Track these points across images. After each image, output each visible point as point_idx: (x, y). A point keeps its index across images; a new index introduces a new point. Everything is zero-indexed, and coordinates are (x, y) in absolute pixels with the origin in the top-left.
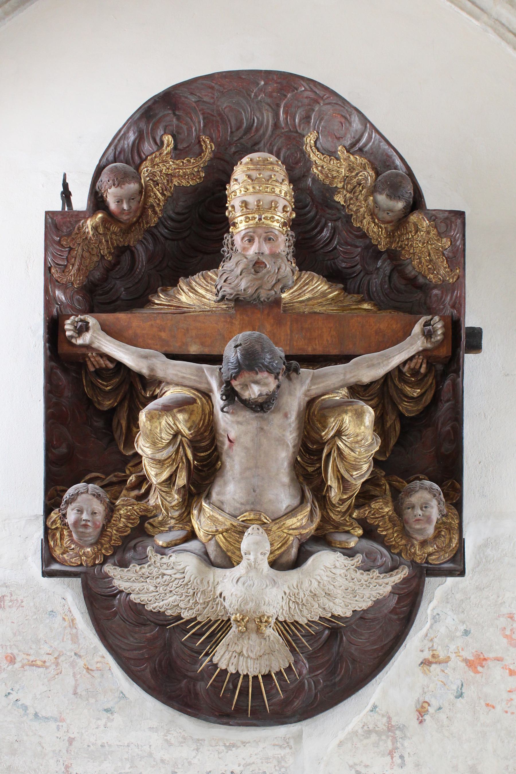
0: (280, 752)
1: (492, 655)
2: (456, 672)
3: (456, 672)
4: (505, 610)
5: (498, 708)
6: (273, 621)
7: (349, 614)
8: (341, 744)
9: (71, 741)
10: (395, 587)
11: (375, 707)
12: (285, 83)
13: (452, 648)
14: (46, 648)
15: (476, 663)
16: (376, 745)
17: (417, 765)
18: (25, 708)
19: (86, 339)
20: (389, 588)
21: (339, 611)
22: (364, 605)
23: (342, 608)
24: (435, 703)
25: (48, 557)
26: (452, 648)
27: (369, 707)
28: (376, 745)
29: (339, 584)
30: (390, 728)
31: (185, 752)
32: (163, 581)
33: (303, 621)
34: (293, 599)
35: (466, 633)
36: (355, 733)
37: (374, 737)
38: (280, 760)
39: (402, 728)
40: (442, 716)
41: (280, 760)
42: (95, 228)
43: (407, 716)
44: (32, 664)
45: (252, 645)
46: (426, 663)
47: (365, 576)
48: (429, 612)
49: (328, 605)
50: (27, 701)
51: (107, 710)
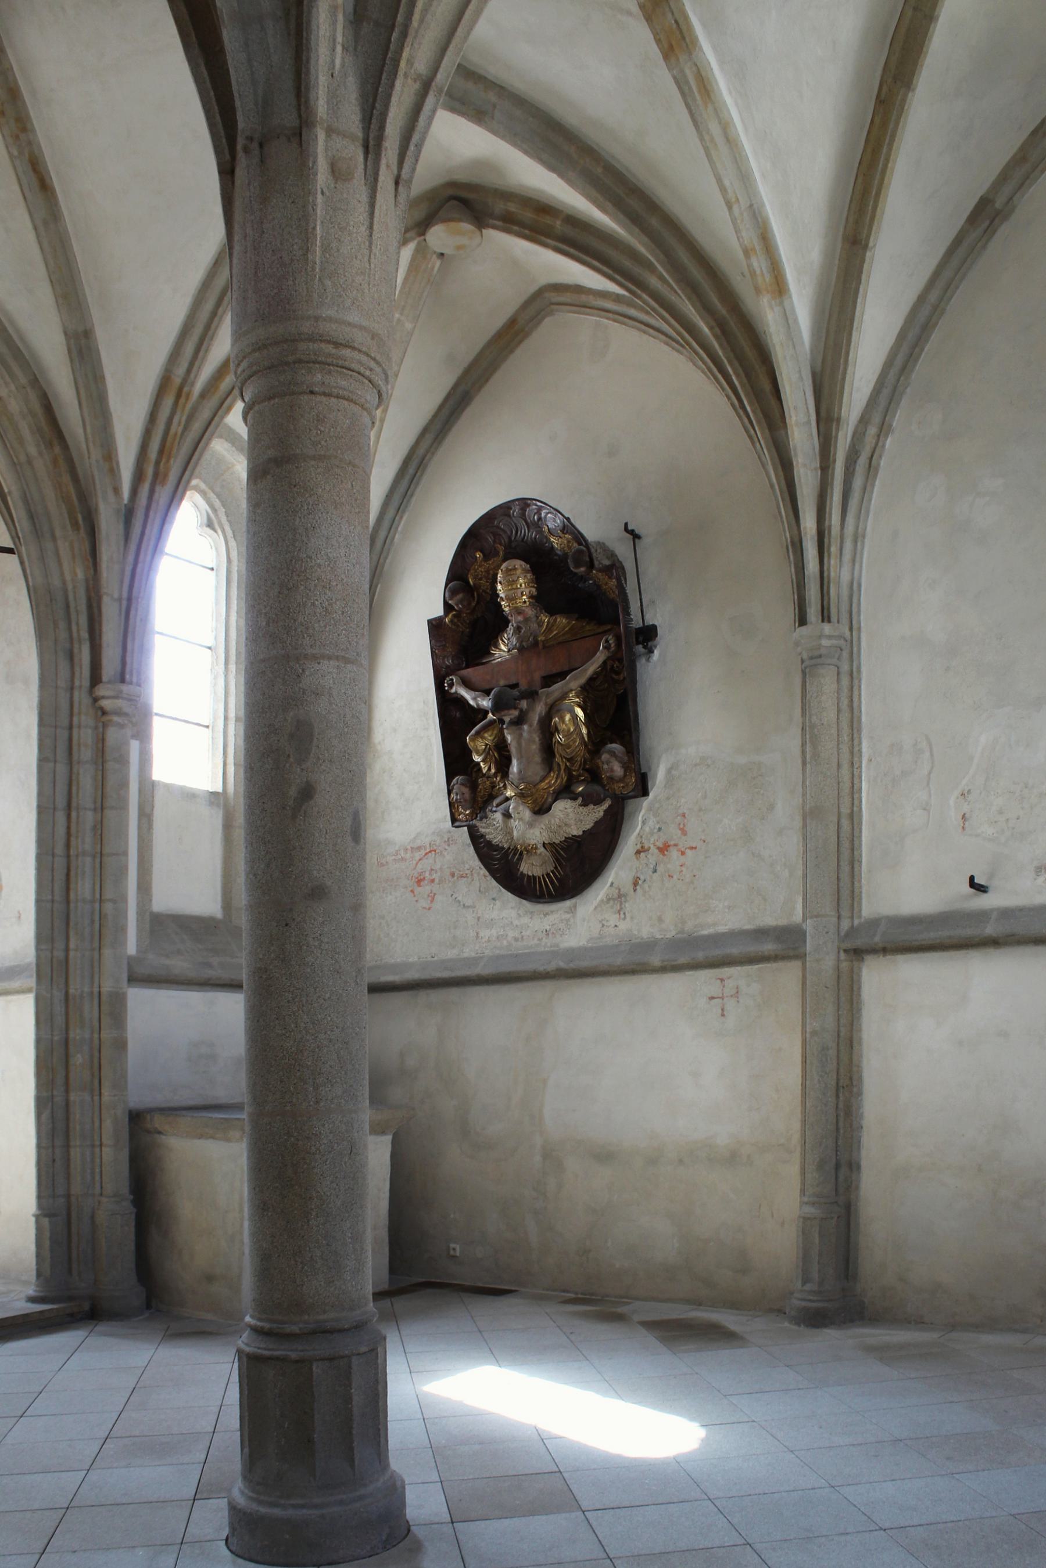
0: (568, 916)
1: (672, 843)
2: (653, 856)
3: (653, 856)
4: (680, 812)
5: (675, 877)
6: (540, 846)
7: (581, 833)
8: (596, 908)
9: (479, 918)
10: (605, 811)
11: (612, 884)
12: (504, 509)
13: (652, 840)
14: (467, 866)
15: (664, 849)
16: (612, 907)
17: (632, 918)
18: (459, 902)
19: (453, 690)
20: (602, 814)
21: (575, 833)
22: (588, 826)
23: (576, 831)
24: (642, 878)
25: (454, 820)
26: (652, 840)
27: (609, 884)
28: (612, 907)
29: (571, 818)
30: (620, 896)
31: (525, 920)
32: (493, 826)
33: (557, 842)
34: (549, 828)
35: (660, 829)
36: (602, 901)
37: (611, 902)
38: (568, 920)
39: (625, 896)
40: (646, 886)
41: (568, 920)
42: (451, 621)
43: (628, 888)
44: (462, 877)
45: (535, 860)
46: (638, 852)
47: (585, 809)
48: (640, 818)
49: (568, 830)
50: (460, 898)
51: (494, 899)
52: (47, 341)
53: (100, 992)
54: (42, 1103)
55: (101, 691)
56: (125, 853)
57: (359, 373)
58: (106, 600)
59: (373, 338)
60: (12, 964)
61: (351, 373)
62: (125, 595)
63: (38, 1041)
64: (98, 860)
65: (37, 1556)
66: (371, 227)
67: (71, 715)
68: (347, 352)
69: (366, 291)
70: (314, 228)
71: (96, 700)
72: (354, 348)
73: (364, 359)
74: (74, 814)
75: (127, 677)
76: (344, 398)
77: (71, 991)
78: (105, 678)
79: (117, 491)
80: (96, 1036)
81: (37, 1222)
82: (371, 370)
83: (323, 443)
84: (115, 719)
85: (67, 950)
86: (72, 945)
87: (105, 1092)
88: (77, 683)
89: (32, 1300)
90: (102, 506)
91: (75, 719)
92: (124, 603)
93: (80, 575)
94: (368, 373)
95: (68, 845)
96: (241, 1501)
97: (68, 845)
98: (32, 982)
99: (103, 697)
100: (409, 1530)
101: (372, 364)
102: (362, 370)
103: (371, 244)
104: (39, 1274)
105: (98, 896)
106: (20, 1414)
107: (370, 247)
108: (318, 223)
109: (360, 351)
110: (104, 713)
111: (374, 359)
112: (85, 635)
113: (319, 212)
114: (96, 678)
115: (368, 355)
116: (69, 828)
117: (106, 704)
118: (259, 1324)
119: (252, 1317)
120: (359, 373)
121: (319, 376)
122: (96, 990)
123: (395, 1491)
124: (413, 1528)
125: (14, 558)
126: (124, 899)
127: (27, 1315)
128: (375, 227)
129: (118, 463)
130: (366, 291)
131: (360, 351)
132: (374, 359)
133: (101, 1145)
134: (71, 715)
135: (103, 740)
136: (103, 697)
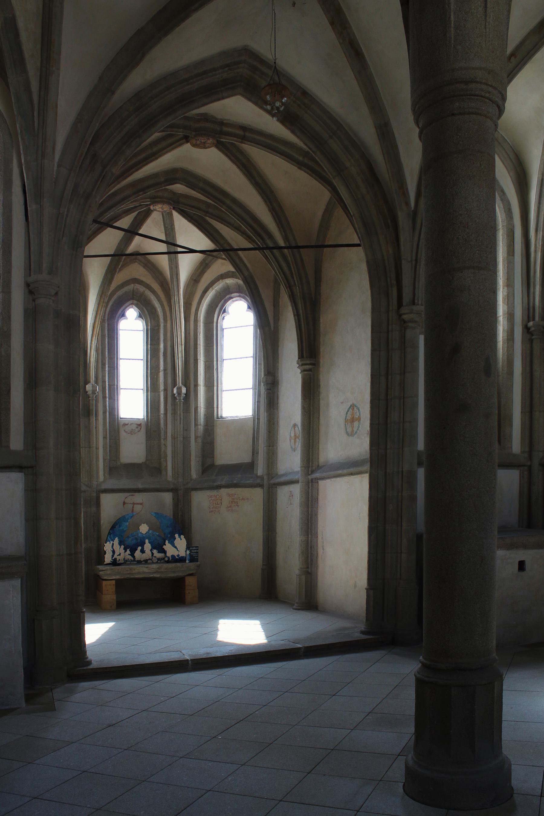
52: (367, 132)
53: (402, 471)
54: (372, 530)
55: (403, 310)
56: (417, 396)
57: (482, 96)
58: (403, 262)
59: (489, 73)
60: (364, 458)
61: (476, 97)
62: (414, 258)
63: (370, 498)
64: (402, 401)
65: (306, 774)
66: (486, 7)
67: (388, 324)
68: (473, 86)
69: (484, 46)
70: (450, 18)
71: (400, 316)
72: (477, 82)
73: (484, 87)
74: (390, 377)
75: (416, 301)
76: (472, 113)
77: (388, 471)
78: (404, 304)
79: (407, 204)
80: (400, 494)
81: (367, 592)
82: (489, 93)
83: (461, 142)
84: (410, 324)
85: (386, 449)
86: (388, 447)
87: (404, 524)
88: (391, 308)
89: (362, 633)
90: (399, 213)
91: (390, 328)
92: (414, 263)
93: (391, 251)
94: (487, 95)
95: (387, 395)
96: (411, 763)
97: (387, 395)
98: (367, 467)
99: (404, 314)
100: (512, 796)
101: (490, 89)
102: (483, 94)
103: (486, 16)
104: (367, 619)
105: (402, 419)
106: (334, 693)
107: (486, 18)
108: (452, 14)
109: (481, 83)
110: (405, 322)
111: (491, 86)
112: (394, 282)
113: (452, 7)
114: (400, 304)
115: (487, 84)
116: (387, 385)
117: (405, 317)
118: (425, 661)
119: (423, 657)
120: (482, 96)
121: (457, 104)
122: (400, 470)
123: (504, 771)
124: (514, 795)
125: (360, 249)
126: (416, 420)
127: (358, 641)
128: (488, 5)
129: (407, 189)
130: (484, 46)
131: (481, 83)
132: (491, 86)
133: (401, 553)
134: (388, 324)
135: (405, 336)
136: (404, 314)
